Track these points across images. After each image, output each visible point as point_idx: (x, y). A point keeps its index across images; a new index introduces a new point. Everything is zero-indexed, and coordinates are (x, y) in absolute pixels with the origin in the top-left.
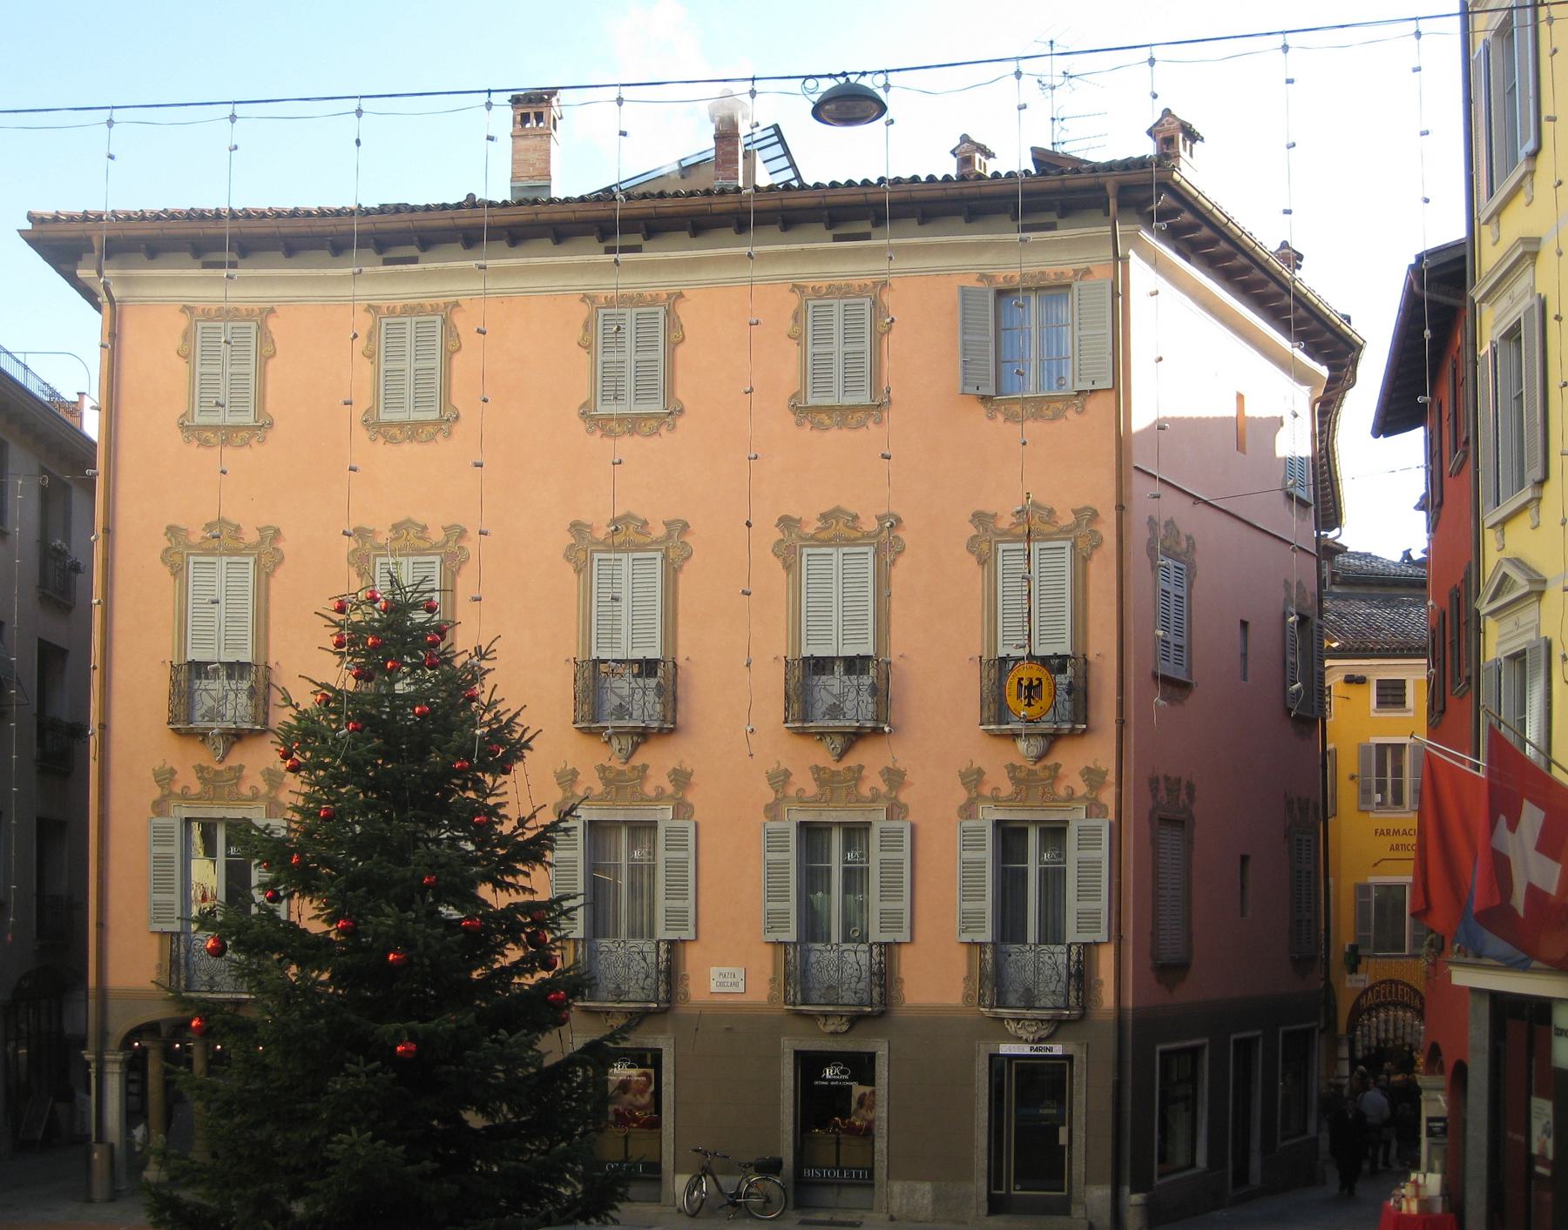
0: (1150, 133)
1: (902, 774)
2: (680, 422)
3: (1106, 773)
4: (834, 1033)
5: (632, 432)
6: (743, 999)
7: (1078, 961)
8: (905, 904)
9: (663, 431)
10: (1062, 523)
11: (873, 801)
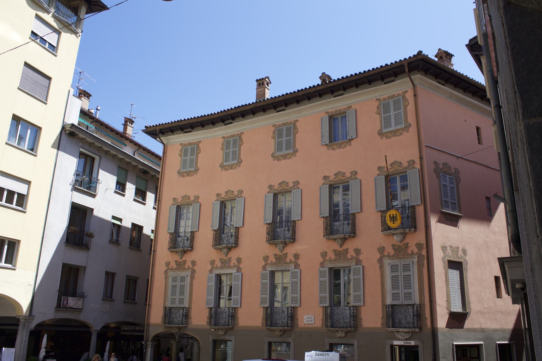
0: (320, 78)
1: (360, 250)
2: (297, 154)
3: (423, 245)
4: (341, 337)
5: (285, 159)
6: (314, 326)
7: (417, 310)
8: (361, 293)
9: (293, 157)
10: (404, 166)
11: (351, 259)
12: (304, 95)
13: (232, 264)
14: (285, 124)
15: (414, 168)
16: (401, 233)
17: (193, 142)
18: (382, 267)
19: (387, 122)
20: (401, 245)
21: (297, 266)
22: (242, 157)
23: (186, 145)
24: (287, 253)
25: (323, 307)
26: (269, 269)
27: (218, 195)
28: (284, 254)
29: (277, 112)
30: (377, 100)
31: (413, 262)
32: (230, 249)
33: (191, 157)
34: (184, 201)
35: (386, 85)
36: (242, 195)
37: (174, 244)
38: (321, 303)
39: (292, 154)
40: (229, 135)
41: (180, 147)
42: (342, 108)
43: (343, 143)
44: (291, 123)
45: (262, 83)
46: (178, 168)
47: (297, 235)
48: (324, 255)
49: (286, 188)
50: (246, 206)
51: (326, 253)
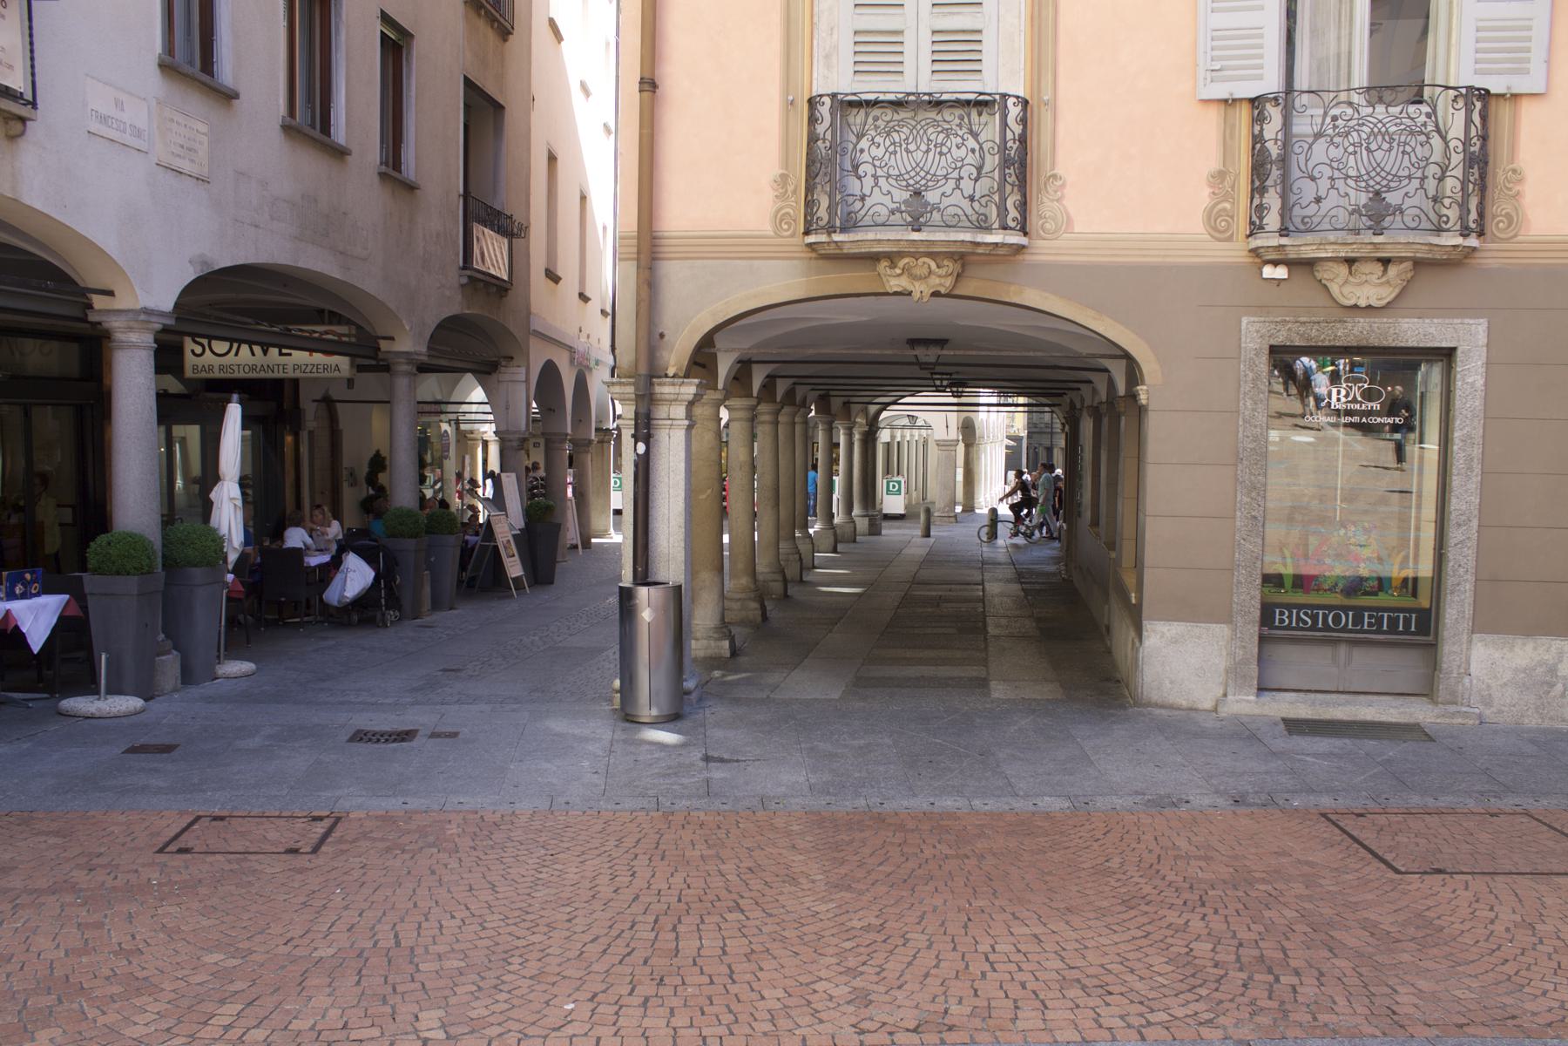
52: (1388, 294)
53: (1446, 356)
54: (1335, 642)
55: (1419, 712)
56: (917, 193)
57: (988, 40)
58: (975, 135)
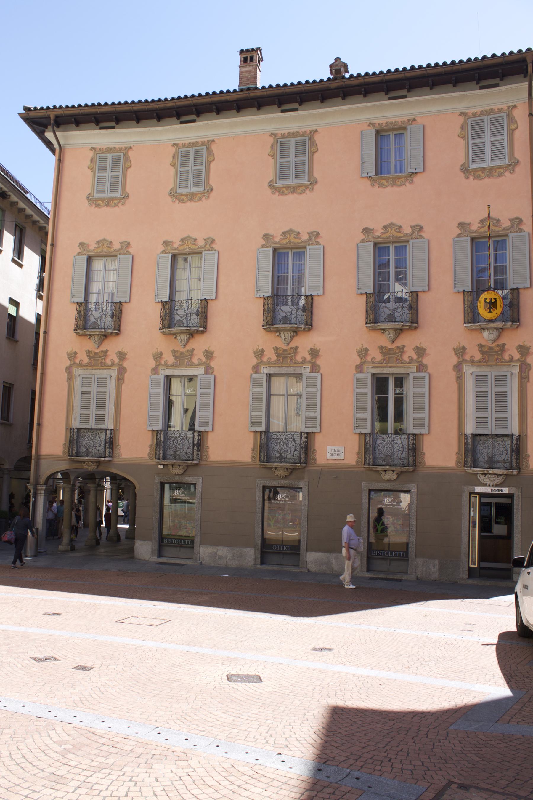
2: (316, 187)
4: (389, 481)
5: (293, 192)
10: (504, 226)
11: (410, 363)
12: (360, 85)
13: (195, 361)
14: (293, 134)
15: (521, 230)
16: (497, 329)
17: (117, 146)
18: (460, 378)
19: (478, 153)
20: (493, 345)
21: (315, 368)
22: (212, 183)
23: (102, 151)
24: (297, 348)
25: (360, 434)
26: (265, 370)
27: (166, 243)
28: (291, 348)
29: (282, 111)
30: (461, 114)
31: (512, 374)
32: (191, 334)
33: (113, 174)
34: (100, 249)
35: (182, 125)
36: (214, 246)
37: (83, 323)
38: (357, 427)
39: (307, 187)
40: (187, 142)
41: (91, 154)
42: (399, 120)
43: (399, 178)
44: (304, 134)
45: (250, 57)
46: (89, 191)
47: (315, 318)
48: (363, 353)
49: (296, 241)
50: (220, 266)
51: (367, 350)
52: (182, 472)
53: (195, 484)
54: (176, 546)
55: (295, 570)
56: (87, 449)
57: (106, 416)
58: (100, 438)
